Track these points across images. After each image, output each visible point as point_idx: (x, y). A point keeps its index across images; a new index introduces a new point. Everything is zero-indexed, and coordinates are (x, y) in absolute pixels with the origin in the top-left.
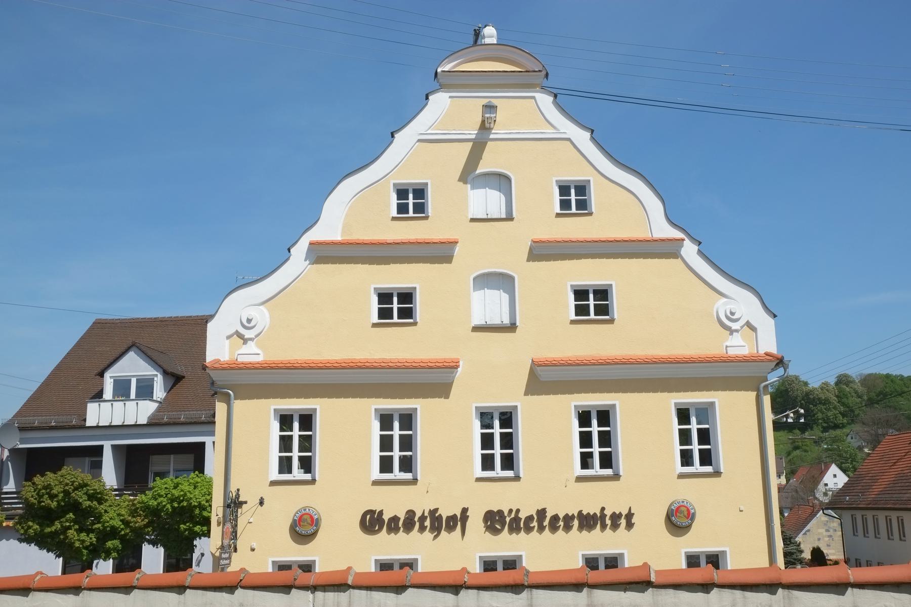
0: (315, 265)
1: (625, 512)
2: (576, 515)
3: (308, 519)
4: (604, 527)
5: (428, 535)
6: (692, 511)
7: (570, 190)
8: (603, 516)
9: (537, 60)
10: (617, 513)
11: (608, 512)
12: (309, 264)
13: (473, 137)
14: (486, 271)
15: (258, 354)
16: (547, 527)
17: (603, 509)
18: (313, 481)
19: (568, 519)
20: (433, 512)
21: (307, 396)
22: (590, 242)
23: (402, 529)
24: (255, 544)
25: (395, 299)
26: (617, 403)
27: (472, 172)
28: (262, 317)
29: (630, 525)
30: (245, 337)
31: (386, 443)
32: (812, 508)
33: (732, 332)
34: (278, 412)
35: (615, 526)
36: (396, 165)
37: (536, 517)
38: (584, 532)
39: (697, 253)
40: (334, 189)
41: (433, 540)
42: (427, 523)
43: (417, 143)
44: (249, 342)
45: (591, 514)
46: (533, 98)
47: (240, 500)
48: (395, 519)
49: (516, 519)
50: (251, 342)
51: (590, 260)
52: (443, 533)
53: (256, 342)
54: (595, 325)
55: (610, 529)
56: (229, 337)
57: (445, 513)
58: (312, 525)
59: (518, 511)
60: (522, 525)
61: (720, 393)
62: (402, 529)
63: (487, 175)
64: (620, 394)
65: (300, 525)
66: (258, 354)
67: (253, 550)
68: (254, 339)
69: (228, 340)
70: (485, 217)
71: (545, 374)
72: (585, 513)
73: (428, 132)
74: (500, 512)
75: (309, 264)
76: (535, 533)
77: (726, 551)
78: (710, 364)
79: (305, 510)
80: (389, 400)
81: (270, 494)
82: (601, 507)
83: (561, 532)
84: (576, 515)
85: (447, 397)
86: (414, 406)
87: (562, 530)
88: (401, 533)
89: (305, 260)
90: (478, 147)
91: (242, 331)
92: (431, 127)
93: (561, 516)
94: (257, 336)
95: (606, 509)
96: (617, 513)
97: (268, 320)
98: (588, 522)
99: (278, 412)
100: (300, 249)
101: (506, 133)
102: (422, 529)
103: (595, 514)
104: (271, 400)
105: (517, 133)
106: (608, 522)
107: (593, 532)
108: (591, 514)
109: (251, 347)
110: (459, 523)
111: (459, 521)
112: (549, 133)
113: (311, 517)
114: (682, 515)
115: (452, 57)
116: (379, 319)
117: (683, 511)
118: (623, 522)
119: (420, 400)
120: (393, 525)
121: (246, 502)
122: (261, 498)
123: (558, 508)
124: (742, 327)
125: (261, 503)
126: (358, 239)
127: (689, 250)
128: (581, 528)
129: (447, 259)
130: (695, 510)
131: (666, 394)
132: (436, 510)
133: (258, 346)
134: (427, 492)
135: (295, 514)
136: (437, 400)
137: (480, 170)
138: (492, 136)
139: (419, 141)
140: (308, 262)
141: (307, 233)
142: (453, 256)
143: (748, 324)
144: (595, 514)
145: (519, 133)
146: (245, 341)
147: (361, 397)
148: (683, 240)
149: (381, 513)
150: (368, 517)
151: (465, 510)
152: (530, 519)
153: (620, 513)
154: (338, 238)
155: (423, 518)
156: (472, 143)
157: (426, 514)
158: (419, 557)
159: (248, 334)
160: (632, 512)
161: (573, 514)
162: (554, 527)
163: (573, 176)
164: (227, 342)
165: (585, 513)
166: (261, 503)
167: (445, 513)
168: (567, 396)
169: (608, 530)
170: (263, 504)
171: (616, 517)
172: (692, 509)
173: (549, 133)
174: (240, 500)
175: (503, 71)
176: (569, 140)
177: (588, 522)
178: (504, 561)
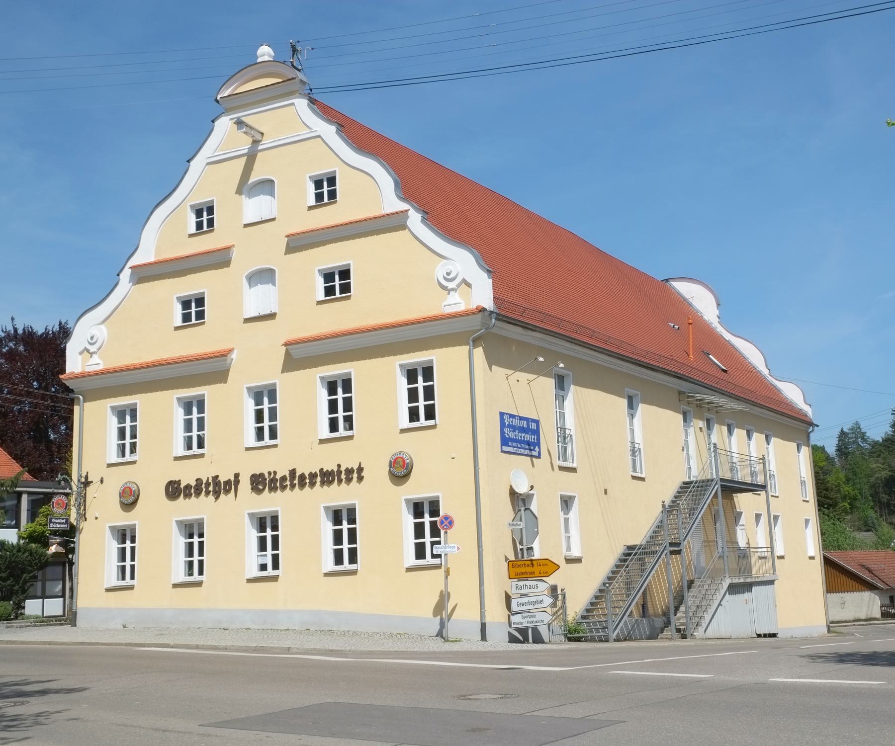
0: (288, 255)
1: (355, 467)
4: (340, 481)
5: (211, 497)
7: (323, 182)
8: (339, 472)
10: (313, 472)
11: (343, 469)
12: (132, 285)
13: (246, 151)
14: (255, 269)
15: (460, 303)
17: (339, 466)
18: (434, 427)
19: (313, 476)
21: (427, 348)
22: (318, 230)
23: (193, 494)
24: (97, 514)
25: (337, 277)
26: (352, 370)
27: (245, 184)
28: (101, 333)
29: (360, 479)
30: (448, 288)
31: (413, 395)
33: (450, 291)
34: (405, 368)
35: (349, 480)
36: (190, 189)
37: (288, 478)
38: (325, 487)
39: (421, 222)
40: (148, 218)
41: (215, 501)
43: (207, 166)
44: (93, 355)
45: (350, 468)
46: (293, 104)
47: (89, 480)
48: (188, 487)
49: (273, 480)
50: (454, 292)
51: (333, 245)
52: (222, 495)
53: (98, 355)
54: (336, 303)
55: (223, 493)
56: (81, 353)
58: (130, 496)
59: (275, 473)
61: (438, 351)
62: (193, 494)
63: (261, 184)
64: (355, 363)
65: (123, 497)
66: (460, 303)
67: (96, 518)
68: (97, 352)
69: (81, 356)
70: (261, 220)
71: (296, 351)
73: (215, 154)
74: (262, 475)
75: (132, 285)
76: (288, 490)
78: (197, 362)
79: (400, 454)
80: (180, 390)
81: (108, 473)
83: (307, 488)
84: (318, 473)
85: (225, 382)
86: (135, 401)
87: (308, 487)
88: (193, 498)
89: (129, 283)
90: (251, 158)
91: (89, 347)
92: (216, 149)
93: (307, 475)
94: (99, 349)
96: (313, 472)
97: (106, 335)
98: (327, 477)
99: (405, 368)
100: (126, 274)
101: (271, 142)
102: (208, 493)
103: (332, 470)
104: (108, 400)
105: (279, 140)
106: (343, 476)
107: (332, 486)
109: (96, 359)
110: (336, 477)
111: (232, 485)
112: (304, 133)
113: (404, 461)
115: (229, 83)
118: (355, 475)
119: (207, 387)
120: (187, 492)
121: (92, 482)
123: (304, 469)
124: (459, 286)
125: (102, 481)
126: (166, 258)
127: (415, 219)
128: (323, 483)
129: (226, 263)
131: (391, 358)
132: (217, 477)
133: (100, 358)
134: (211, 462)
136: (218, 385)
137: (253, 179)
138: (260, 147)
139: (208, 164)
140: (131, 284)
141: (131, 260)
142: (231, 260)
143: (464, 281)
144: (332, 470)
145: (280, 139)
146: (91, 354)
147: (167, 390)
148: (406, 211)
151: (237, 476)
152: (284, 479)
153: (352, 468)
154: (152, 260)
156: (246, 157)
157: (210, 481)
158: (205, 517)
159: (93, 349)
161: (352, 468)
162: (302, 485)
163: (322, 170)
164: (80, 357)
166: (102, 481)
168: (313, 369)
169: (343, 484)
171: (349, 472)
173: (303, 134)
174: (89, 480)
175: (256, 89)
176: (319, 136)
177: (327, 477)
178: (348, 509)
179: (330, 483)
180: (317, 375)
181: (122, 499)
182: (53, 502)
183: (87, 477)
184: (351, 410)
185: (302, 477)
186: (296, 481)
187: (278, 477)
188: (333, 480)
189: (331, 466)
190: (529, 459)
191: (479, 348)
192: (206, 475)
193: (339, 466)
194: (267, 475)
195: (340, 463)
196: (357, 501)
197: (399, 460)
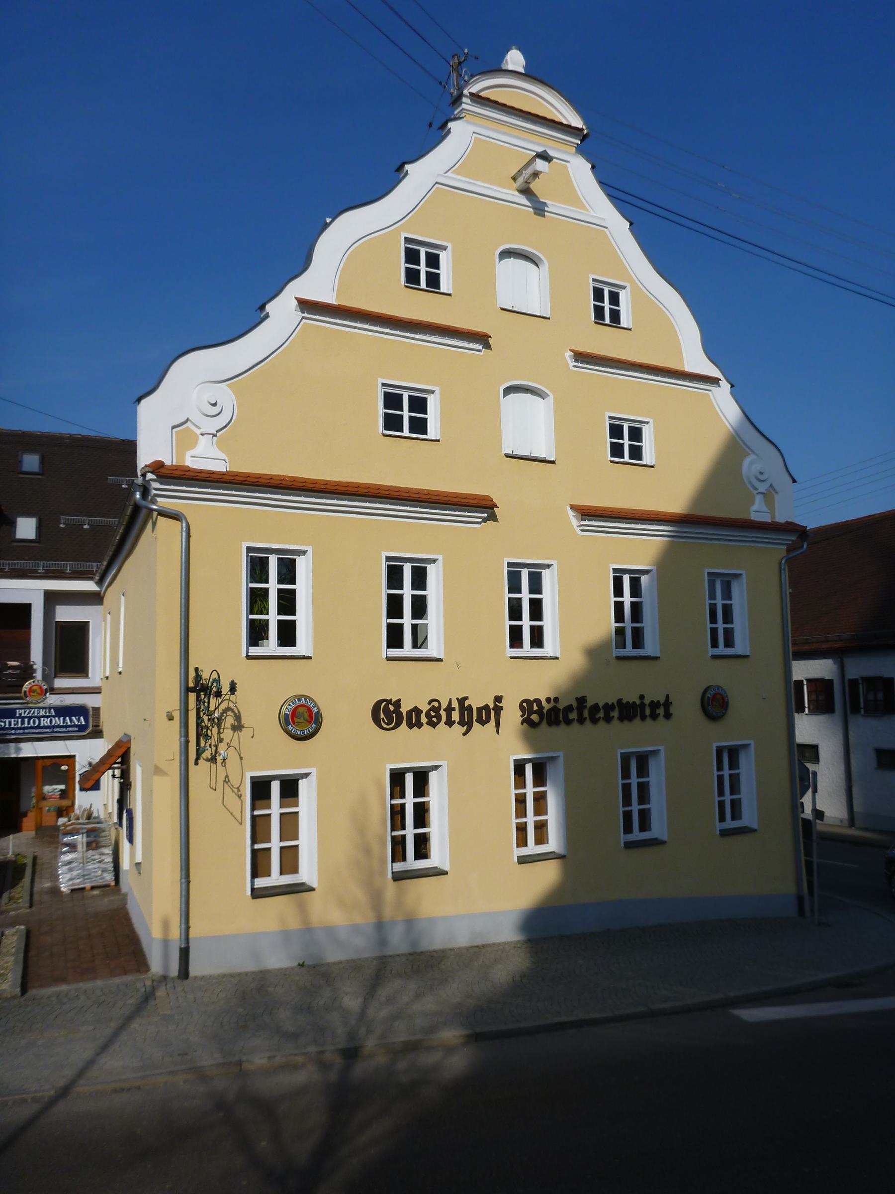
2: (615, 704)
3: (305, 713)
5: (458, 729)
6: (315, 710)
8: (643, 705)
9: (400, 17)
11: (647, 701)
16: (588, 718)
17: (642, 697)
19: (608, 708)
20: (461, 701)
32: (42, 719)
42: (455, 716)
45: (610, 704)
57: (475, 703)
58: (310, 722)
60: (561, 718)
72: (624, 701)
77: (717, 747)
79: (299, 700)
82: (639, 695)
84: (615, 704)
93: (601, 705)
95: (471, 704)
106: (648, 711)
108: (610, 704)
114: (302, 720)
116: (410, 433)
117: (303, 713)
120: (414, 719)
122: (233, 681)
127: (725, 385)
128: (621, 719)
130: (318, 708)
135: (315, 702)
149: (398, 704)
150: (383, 704)
152: (569, 709)
155: (449, 709)
157: (455, 704)
160: (670, 701)
165: (624, 701)
167: (475, 703)
170: (236, 691)
171: (654, 705)
172: (314, 707)
179: (630, 719)
180: (556, 562)
181: (290, 727)
182: (383, 719)
183: (198, 677)
184: (540, 619)
185: (595, 708)
186: (586, 714)
187: (647, 701)
188: (488, 720)
189: (631, 697)
190: (225, 730)
191: (19, 538)
192: (447, 695)
193: (642, 697)
194: (544, 703)
195: (642, 694)
196: (663, 747)
197: (718, 697)
